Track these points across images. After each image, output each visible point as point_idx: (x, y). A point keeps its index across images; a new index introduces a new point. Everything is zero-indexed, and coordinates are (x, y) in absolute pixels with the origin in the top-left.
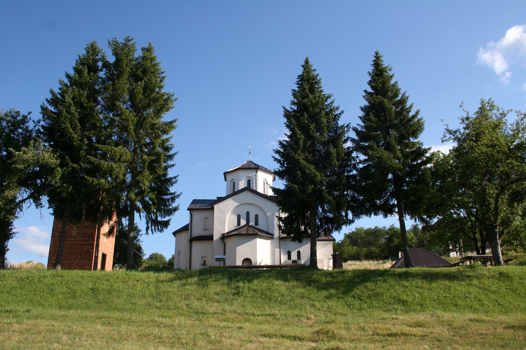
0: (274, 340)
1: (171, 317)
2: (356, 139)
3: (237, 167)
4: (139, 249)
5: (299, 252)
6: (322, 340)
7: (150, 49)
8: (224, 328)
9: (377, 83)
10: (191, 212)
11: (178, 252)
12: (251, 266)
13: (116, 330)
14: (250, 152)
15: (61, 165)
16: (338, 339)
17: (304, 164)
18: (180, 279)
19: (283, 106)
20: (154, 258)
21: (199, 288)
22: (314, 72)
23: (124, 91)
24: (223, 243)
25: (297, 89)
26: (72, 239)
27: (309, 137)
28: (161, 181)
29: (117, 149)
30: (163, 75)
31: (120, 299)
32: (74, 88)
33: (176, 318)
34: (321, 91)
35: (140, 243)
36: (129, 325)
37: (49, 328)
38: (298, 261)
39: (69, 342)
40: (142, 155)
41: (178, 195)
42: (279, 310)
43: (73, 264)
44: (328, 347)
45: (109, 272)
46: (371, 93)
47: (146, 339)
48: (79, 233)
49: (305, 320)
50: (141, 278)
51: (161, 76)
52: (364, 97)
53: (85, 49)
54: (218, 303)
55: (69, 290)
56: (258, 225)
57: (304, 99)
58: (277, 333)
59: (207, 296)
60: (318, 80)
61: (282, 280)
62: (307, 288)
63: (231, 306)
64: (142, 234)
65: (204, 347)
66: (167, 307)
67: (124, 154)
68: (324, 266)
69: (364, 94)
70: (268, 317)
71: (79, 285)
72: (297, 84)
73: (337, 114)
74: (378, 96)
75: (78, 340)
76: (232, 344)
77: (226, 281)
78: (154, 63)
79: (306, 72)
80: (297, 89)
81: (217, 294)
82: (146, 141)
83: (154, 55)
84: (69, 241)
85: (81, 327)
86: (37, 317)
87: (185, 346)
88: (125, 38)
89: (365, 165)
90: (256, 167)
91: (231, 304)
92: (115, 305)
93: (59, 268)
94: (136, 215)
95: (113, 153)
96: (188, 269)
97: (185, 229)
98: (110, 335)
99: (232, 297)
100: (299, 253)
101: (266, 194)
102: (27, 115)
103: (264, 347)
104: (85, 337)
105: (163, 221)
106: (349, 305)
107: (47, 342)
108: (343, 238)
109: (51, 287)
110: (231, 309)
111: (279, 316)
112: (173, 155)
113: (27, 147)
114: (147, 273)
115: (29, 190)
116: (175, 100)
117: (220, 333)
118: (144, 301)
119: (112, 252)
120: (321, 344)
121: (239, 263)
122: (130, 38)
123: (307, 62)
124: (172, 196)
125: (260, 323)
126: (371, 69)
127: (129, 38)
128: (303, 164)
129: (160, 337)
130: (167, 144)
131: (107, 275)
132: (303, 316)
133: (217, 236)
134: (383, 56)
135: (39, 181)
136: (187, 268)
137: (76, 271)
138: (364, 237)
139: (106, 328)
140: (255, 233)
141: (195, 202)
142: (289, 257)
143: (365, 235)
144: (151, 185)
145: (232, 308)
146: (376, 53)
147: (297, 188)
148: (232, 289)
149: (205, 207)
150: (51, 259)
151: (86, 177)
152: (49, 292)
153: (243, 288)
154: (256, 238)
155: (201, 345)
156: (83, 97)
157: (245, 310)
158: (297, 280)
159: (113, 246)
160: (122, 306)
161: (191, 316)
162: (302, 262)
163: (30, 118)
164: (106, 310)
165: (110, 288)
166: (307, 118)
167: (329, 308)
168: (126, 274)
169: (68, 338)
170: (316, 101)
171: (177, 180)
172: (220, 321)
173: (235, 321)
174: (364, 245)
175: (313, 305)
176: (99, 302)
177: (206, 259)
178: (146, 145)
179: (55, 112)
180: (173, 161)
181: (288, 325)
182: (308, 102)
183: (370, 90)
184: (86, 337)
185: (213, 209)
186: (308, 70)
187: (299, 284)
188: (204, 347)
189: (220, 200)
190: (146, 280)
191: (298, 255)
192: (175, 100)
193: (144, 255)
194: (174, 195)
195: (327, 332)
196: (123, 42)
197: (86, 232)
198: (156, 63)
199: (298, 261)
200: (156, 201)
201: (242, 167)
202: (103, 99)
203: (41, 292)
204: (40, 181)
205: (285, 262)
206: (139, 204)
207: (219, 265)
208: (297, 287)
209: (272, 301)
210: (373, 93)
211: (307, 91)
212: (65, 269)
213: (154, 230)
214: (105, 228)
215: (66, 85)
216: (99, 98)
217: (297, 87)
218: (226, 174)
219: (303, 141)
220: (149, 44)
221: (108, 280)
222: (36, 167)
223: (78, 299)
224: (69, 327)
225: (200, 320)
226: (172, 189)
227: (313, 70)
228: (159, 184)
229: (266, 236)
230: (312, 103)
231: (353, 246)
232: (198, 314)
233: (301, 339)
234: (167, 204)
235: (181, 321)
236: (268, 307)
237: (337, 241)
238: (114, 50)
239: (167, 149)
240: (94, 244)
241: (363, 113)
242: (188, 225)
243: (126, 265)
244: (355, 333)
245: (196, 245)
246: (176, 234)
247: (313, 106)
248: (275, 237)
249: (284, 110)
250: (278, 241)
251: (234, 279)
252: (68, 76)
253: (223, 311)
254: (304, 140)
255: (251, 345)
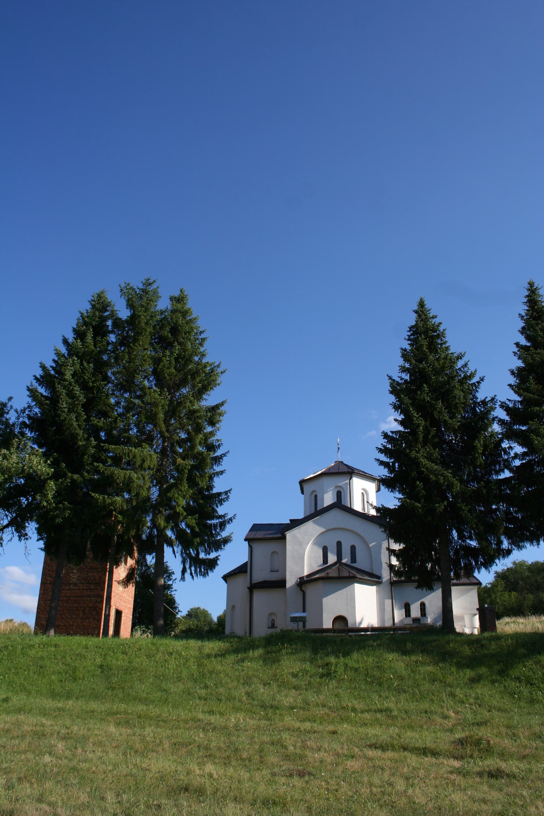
0: (390, 754)
1: (223, 714)
2: (507, 421)
3: (320, 472)
4: (171, 602)
5: (423, 605)
6: (471, 756)
7: (182, 297)
8: (309, 732)
9: (535, 330)
10: (251, 544)
11: (231, 607)
12: (347, 628)
13: (137, 734)
14: (339, 448)
15: (56, 477)
16: (498, 753)
17: (427, 466)
18: (236, 651)
19: (388, 375)
20: (193, 616)
21: (265, 665)
22: (434, 321)
23: (145, 361)
24: (302, 593)
25: (408, 348)
26: (71, 587)
27: (435, 422)
28: (205, 497)
29: (136, 451)
30: (203, 336)
31: (143, 683)
32: (74, 360)
33: (230, 715)
34: (447, 348)
35: (173, 593)
36: (157, 726)
37: (38, 728)
38: (421, 618)
39: (67, 753)
40: (175, 458)
41: (230, 519)
42: (396, 702)
43: (73, 625)
44: (482, 769)
45: (126, 639)
46: (526, 346)
47: (185, 750)
48: (82, 578)
49: (439, 720)
50: (175, 650)
51: (200, 337)
52: (515, 353)
53: (89, 302)
54: (297, 690)
55: (67, 668)
56: (355, 562)
57: (421, 362)
58: (395, 742)
59: (278, 679)
60: (442, 331)
61: (397, 652)
62: (440, 665)
63: (318, 696)
64: (176, 579)
65: (277, 766)
66: (216, 697)
67: (148, 458)
68: (465, 626)
69: (516, 349)
70: (378, 714)
71: (82, 659)
72: (408, 340)
73: (474, 383)
74: (539, 351)
75: (80, 751)
76: (321, 762)
77: (308, 654)
78: (188, 318)
79: (422, 320)
80: (408, 348)
81: (295, 676)
82: (180, 437)
83: (188, 306)
84: (66, 590)
85: (84, 728)
86: (19, 711)
87: (247, 762)
88: (144, 281)
89: (524, 462)
90: (350, 470)
91: (317, 692)
92: (135, 692)
93: (52, 632)
94: (168, 550)
95: (131, 457)
96: (248, 634)
97: (242, 570)
98: (129, 744)
99: (319, 680)
100: (423, 606)
101: (366, 512)
102: (7, 401)
103: (374, 766)
104: (91, 745)
105: (208, 559)
106: (512, 694)
107: (34, 752)
108: (494, 579)
109: (40, 663)
110: (318, 701)
111: (395, 713)
112: (221, 457)
113: (8, 449)
114: (185, 641)
115: (10, 512)
116: (222, 373)
117: (302, 742)
118: (181, 686)
119: (130, 608)
120: (470, 763)
121: (328, 624)
122: (150, 281)
123: (422, 304)
124: (220, 520)
125: (366, 725)
126: (523, 309)
127: (150, 281)
128: (425, 465)
129: (207, 748)
130: (211, 439)
131: (123, 644)
132: (436, 713)
133: (291, 581)
134: (540, 288)
135: (24, 500)
136: (246, 633)
137: (77, 639)
138: (528, 576)
139: (123, 730)
140: (351, 575)
141: (256, 528)
142: (408, 613)
143: (529, 574)
144: (188, 504)
145: (319, 698)
146: (529, 284)
147: (419, 508)
148: (319, 667)
149: (272, 536)
150: (39, 617)
151: (93, 494)
152: (37, 671)
153: (336, 665)
154: (354, 583)
155: (272, 763)
156: (88, 373)
157: (340, 701)
158: (422, 652)
159: (132, 597)
160: (147, 694)
161: (254, 712)
162: (429, 620)
163: (11, 407)
164: (121, 701)
165: (128, 664)
166: (428, 393)
167: (477, 698)
168: (153, 643)
169: (65, 746)
170: (439, 364)
171: (228, 496)
172: (301, 721)
173: (325, 720)
174: (528, 590)
175: (452, 694)
176: (111, 688)
177: (273, 617)
178: (181, 442)
179: (47, 396)
180: (220, 466)
181: (411, 727)
182: (428, 367)
183: (524, 342)
184: (93, 745)
185: (284, 538)
186: (423, 317)
187: (428, 660)
188: (277, 766)
189: (295, 523)
190: (183, 653)
191: (421, 609)
192: (222, 373)
193: (179, 611)
194: (224, 518)
195: (478, 742)
196: (141, 286)
197: (92, 576)
198: (191, 318)
199: (421, 618)
200: (197, 530)
201: (328, 472)
202: (113, 374)
203: (25, 671)
204: (25, 499)
205: (401, 621)
206: (169, 533)
207: (296, 628)
208: (423, 664)
209: (384, 688)
210: (529, 347)
211: (424, 349)
212: (61, 633)
213: (195, 573)
214: (121, 572)
215: (63, 356)
216: (109, 374)
217: (409, 344)
218: (303, 484)
219: (423, 429)
220: (181, 291)
221: (124, 653)
222: (19, 478)
223: (81, 681)
224: (67, 728)
225: (269, 719)
226: (221, 510)
227: (431, 316)
228: (201, 501)
229: (369, 580)
230: (434, 369)
231: (510, 591)
232: (265, 709)
233: (435, 754)
234: (214, 532)
235: (239, 720)
236: (377, 697)
237: (484, 585)
238: (128, 300)
239: (212, 448)
240: (104, 594)
241: (515, 379)
242: (245, 564)
243: (151, 627)
244: (526, 745)
245: (259, 597)
246: (227, 579)
247: (437, 373)
248: (384, 580)
249: (390, 380)
250: (388, 588)
251: (321, 652)
252: (65, 341)
253: (305, 704)
254: (426, 428)
255: (353, 764)
